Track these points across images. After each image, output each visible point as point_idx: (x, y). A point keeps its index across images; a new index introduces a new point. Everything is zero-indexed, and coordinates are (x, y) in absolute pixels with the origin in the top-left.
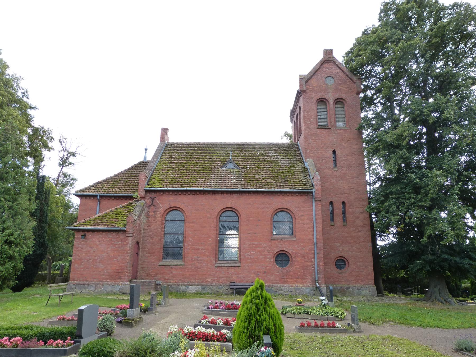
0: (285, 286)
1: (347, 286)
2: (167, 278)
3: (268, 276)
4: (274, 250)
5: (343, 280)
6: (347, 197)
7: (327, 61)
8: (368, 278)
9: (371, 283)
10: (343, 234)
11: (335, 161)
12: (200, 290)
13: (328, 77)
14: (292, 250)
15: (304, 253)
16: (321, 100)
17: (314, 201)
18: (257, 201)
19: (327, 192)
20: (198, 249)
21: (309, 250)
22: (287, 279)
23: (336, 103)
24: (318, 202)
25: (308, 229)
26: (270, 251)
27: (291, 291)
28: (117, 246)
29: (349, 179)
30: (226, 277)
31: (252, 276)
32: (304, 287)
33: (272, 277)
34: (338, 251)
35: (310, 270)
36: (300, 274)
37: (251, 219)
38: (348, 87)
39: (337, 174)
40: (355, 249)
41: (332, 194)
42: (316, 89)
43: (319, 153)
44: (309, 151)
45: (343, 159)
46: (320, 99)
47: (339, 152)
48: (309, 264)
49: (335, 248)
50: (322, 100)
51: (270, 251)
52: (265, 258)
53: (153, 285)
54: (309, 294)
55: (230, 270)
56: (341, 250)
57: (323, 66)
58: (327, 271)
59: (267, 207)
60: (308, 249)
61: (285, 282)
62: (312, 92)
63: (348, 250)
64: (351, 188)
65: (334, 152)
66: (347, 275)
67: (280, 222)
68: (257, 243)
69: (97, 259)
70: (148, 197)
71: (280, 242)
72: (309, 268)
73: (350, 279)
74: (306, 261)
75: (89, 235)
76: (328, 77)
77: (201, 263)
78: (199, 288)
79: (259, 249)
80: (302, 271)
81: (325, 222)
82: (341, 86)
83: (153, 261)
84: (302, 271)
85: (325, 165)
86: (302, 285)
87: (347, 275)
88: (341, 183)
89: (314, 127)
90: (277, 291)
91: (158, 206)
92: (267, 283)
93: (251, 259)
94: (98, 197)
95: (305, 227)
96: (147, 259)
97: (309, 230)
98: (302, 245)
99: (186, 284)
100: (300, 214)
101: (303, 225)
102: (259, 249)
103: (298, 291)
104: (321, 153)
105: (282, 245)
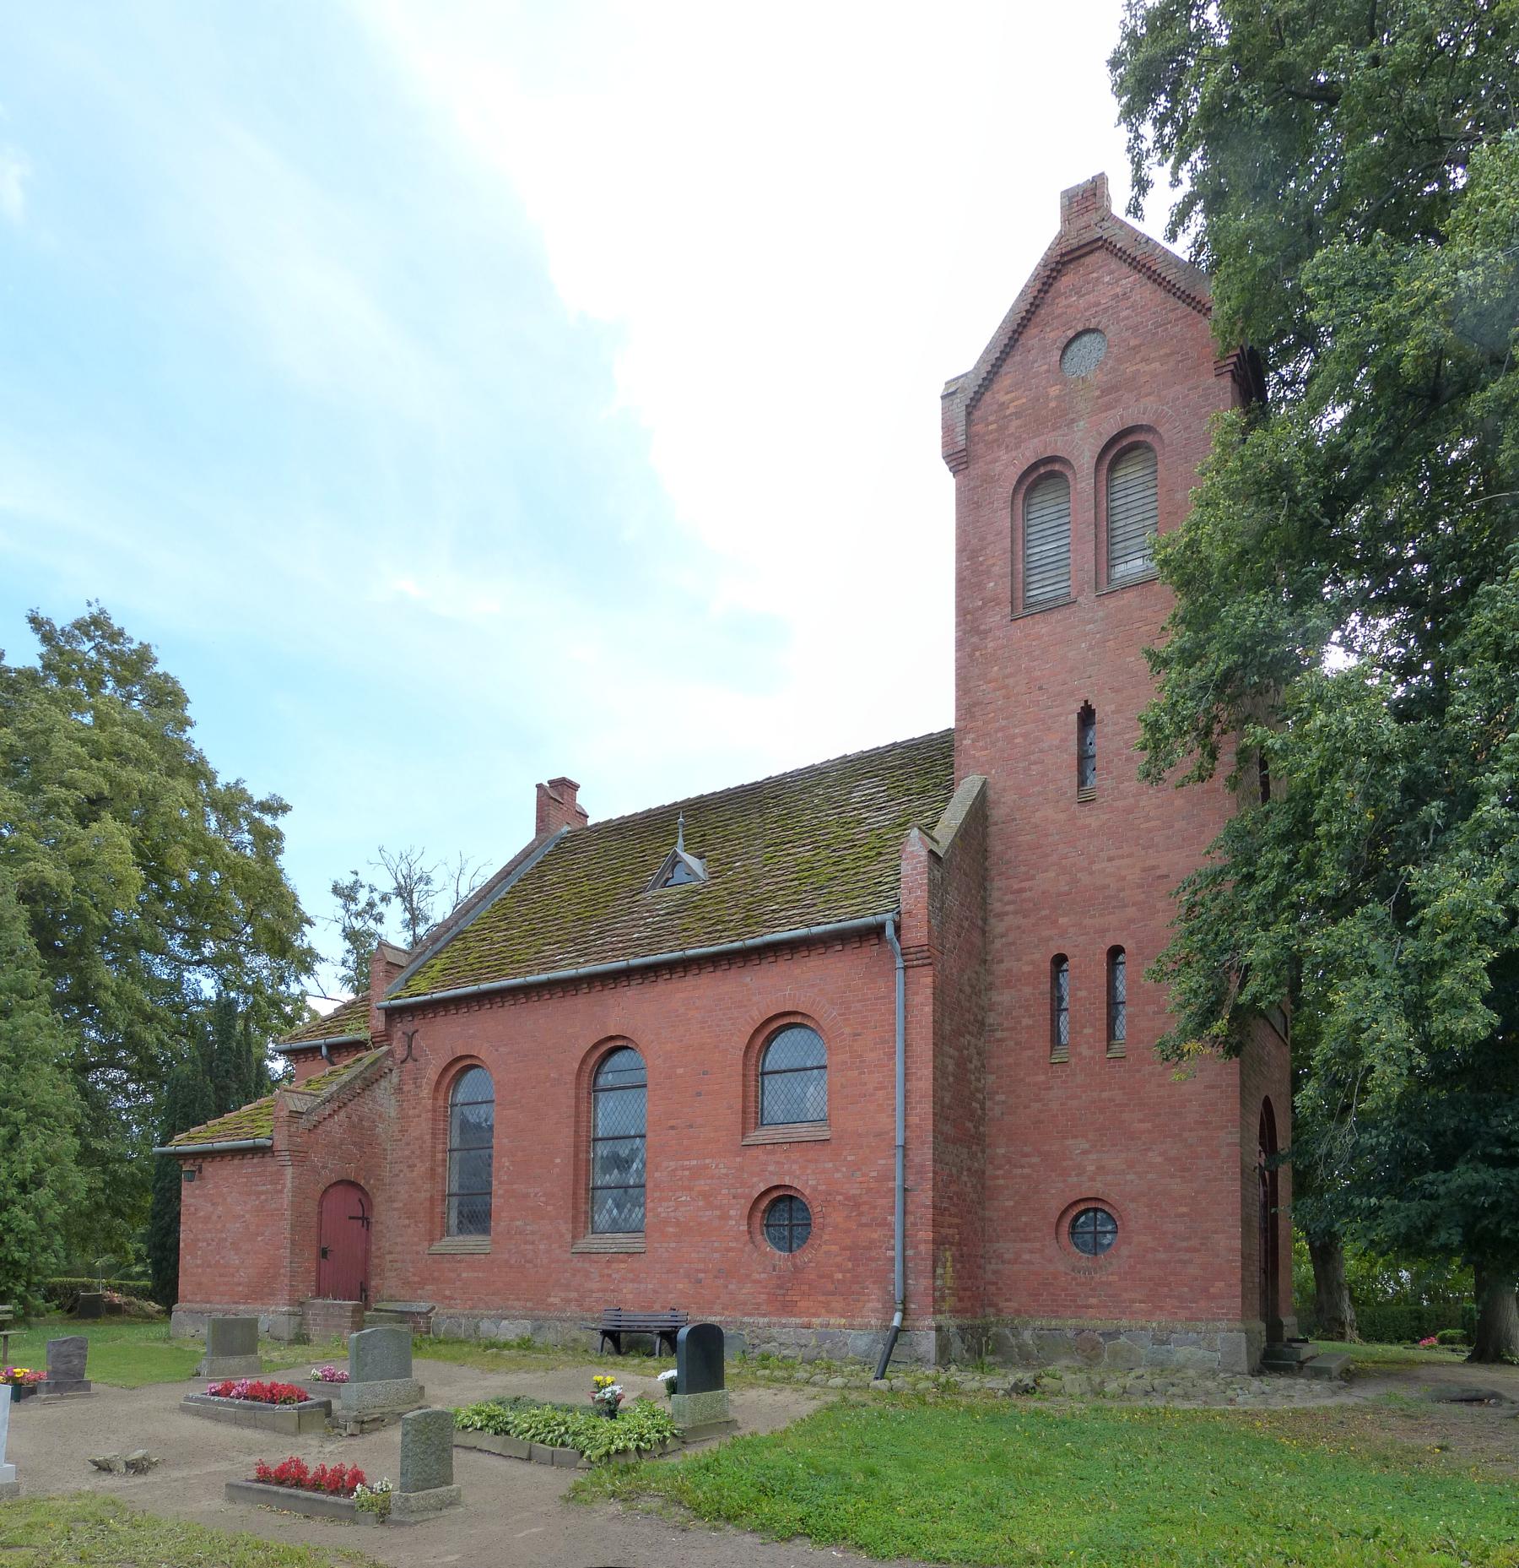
0: (784, 1326)
1: (1110, 1325)
2: (447, 1293)
3: (730, 1287)
4: (752, 1187)
5: (1093, 1301)
6: (1132, 921)
7: (1072, 251)
8: (1212, 1290)
9: (1226, 1314)
10: (1105, 1095)
11: (1084, 759)
12: (527, 1335)
13: (1078, 335)
14: (814, 1182)
15: (858, 1192)
16: (1042, 470)
17: (899, 963)
18: (698, 998)
19: (1044, 913)
20: (526, 1196)
21: (876, 1179)
22: (795, 1298)
23: (1112, 468)
24: (917, 966)
25: (876, 1089)
26: (739, 1191)
27: (803, 1342)
28: (263, 1197)
29: (1150, 831)
30: (604, 1290)
31: (680, 1286)
32: (852, 1327)
33: (744, 1291)
34: (1077, 1175)
35: (878, 1259)
36: (840, 1276)
37: (680, 1071)
38: (1172, 354)
39: (1092, 818)
40: (1159, 1159)
41: (1061, 920)
42: (1018, 422)
43: (1014, 737)
44: (974, 741)
45: (1127, 736)
46: (1034, 467)
47: (1110, 708)
48: (875, 1236)
49: (1065, 1164)
50: (1049, 468)
51: (739, 1191)
52: (721, 1218)
53: (347, 1317)
54: (867, 1357)
55: (615, 1266)
56: (1093, 1168)
57: (1052, 290)
58: (1030, 1263)
59: (730, 1019)
60: (875, 1174)
61: (787, 1308)
62: (999, 446)
63: (1124, 1167)
64: (1159, 872)
65: (1087, 716)
66: (1111, 1278)
67: (785, 1071)
68: (694, 1162)
69: (226, 1239)
70: (400, 1033)
71: (772, 1152)
72: (873, 1254)
73: (1125, 1296)
74: (865, 1225)
75: (209, 1168)
76: (1078, 335)
77: (533, 1243)
78: (526, 1328)
79: (702, 1184)
80: (850, 1265)
81: (1029, 1053)
82: (1138, 358)
83: (416, 1239)
84: (850, 1265)
85: (1038, 788)
86: (843, 1321)
87: (1111, 1278)
88: (1110, 859)
89: (998, 618)
90: (757, 1341)
91: (422, 1060)
92: (726, 1313)
93: (678, 1224)
94: (324, 1051)
95: (865, 1084)
96: (401, 1236)
97: (880, 1093)
98: (853, 1158)
99: (493, 1313)
100: (847, 1030)
101: (860, 1073)
102: (702, 1184)
103: (827, 1345)
104: (1025, 736)
105: (778, 1163)
